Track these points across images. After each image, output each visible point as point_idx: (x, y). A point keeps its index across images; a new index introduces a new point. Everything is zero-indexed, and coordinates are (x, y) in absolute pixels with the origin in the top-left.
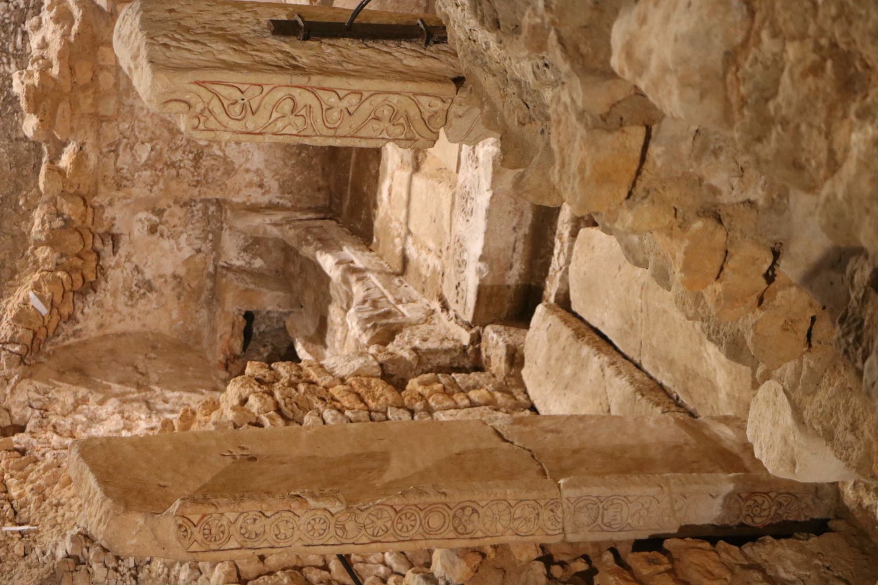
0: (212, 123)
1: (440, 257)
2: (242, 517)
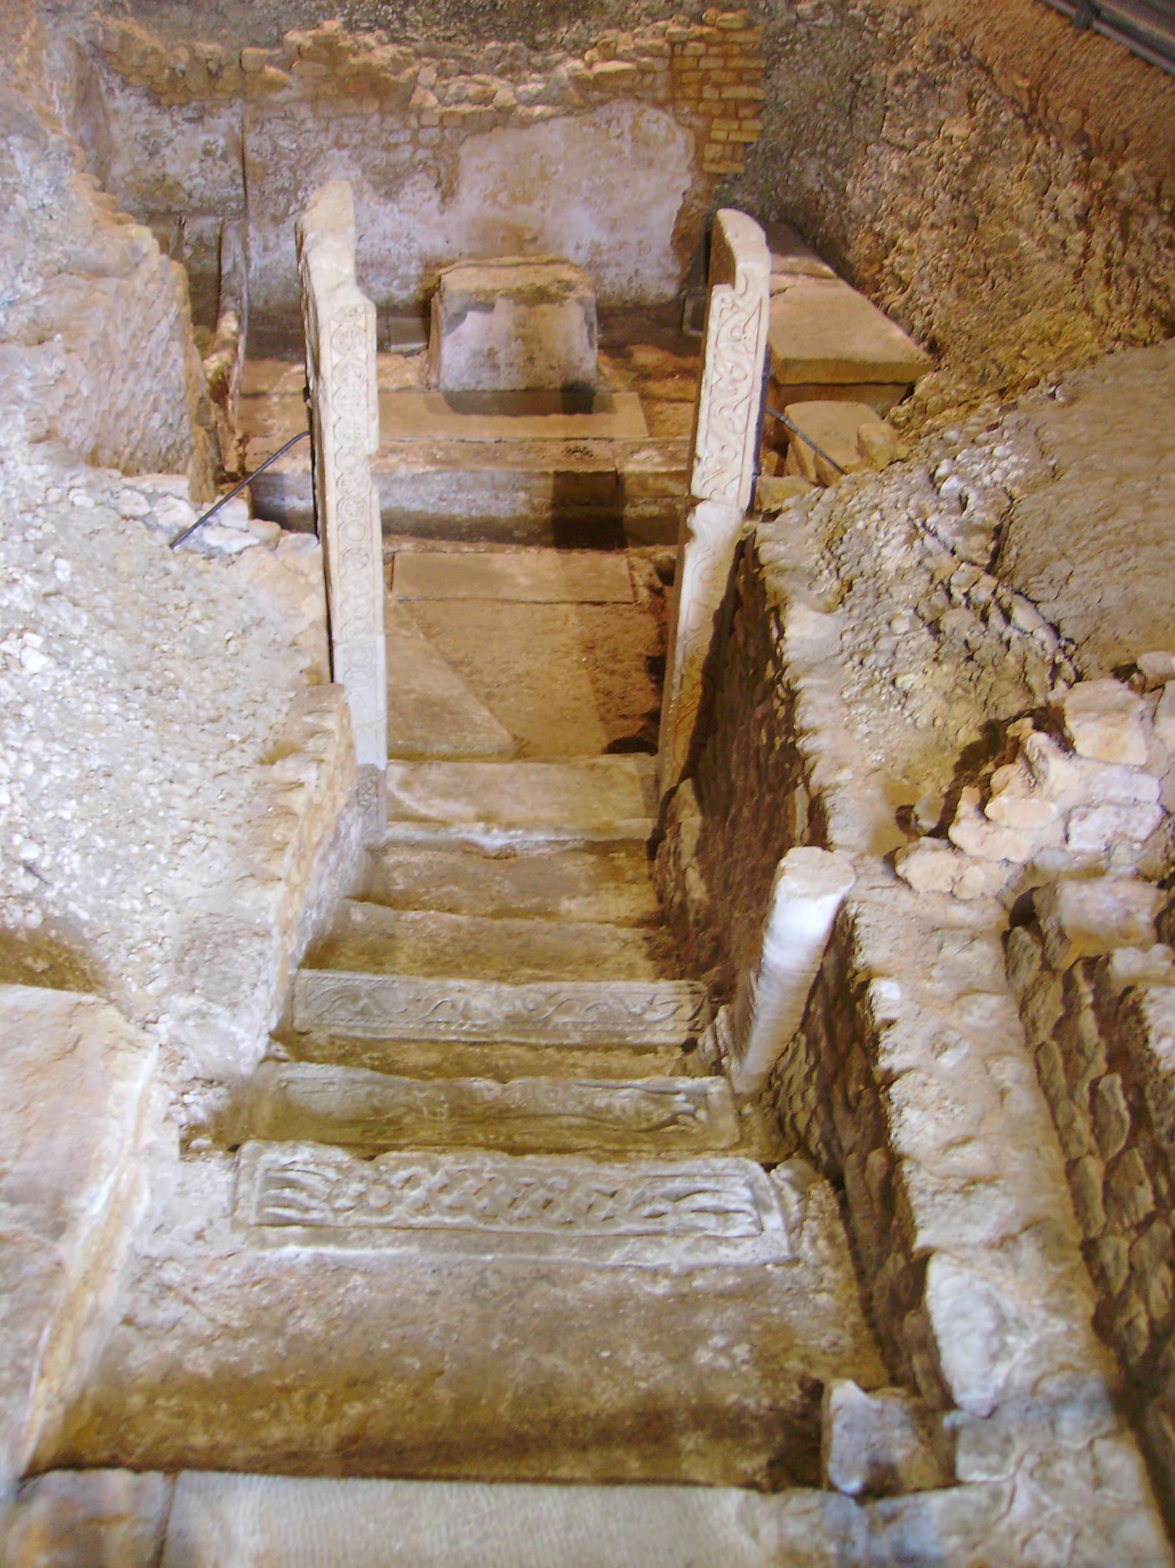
0: (726, 314)
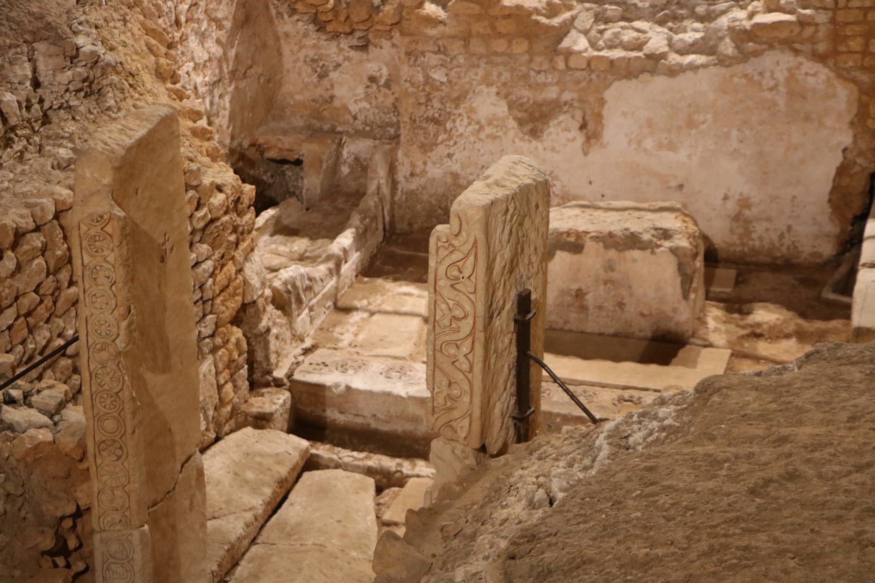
0: (443, 253)
1: (350, 345)
2: (110, 267)
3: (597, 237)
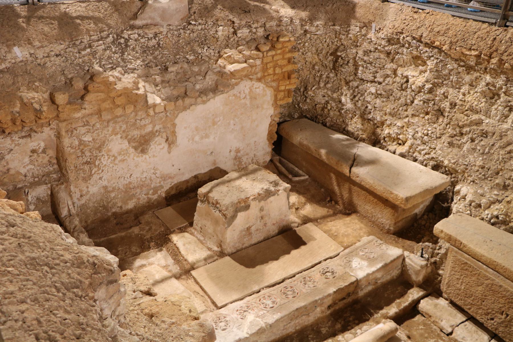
3: (255, 198)
